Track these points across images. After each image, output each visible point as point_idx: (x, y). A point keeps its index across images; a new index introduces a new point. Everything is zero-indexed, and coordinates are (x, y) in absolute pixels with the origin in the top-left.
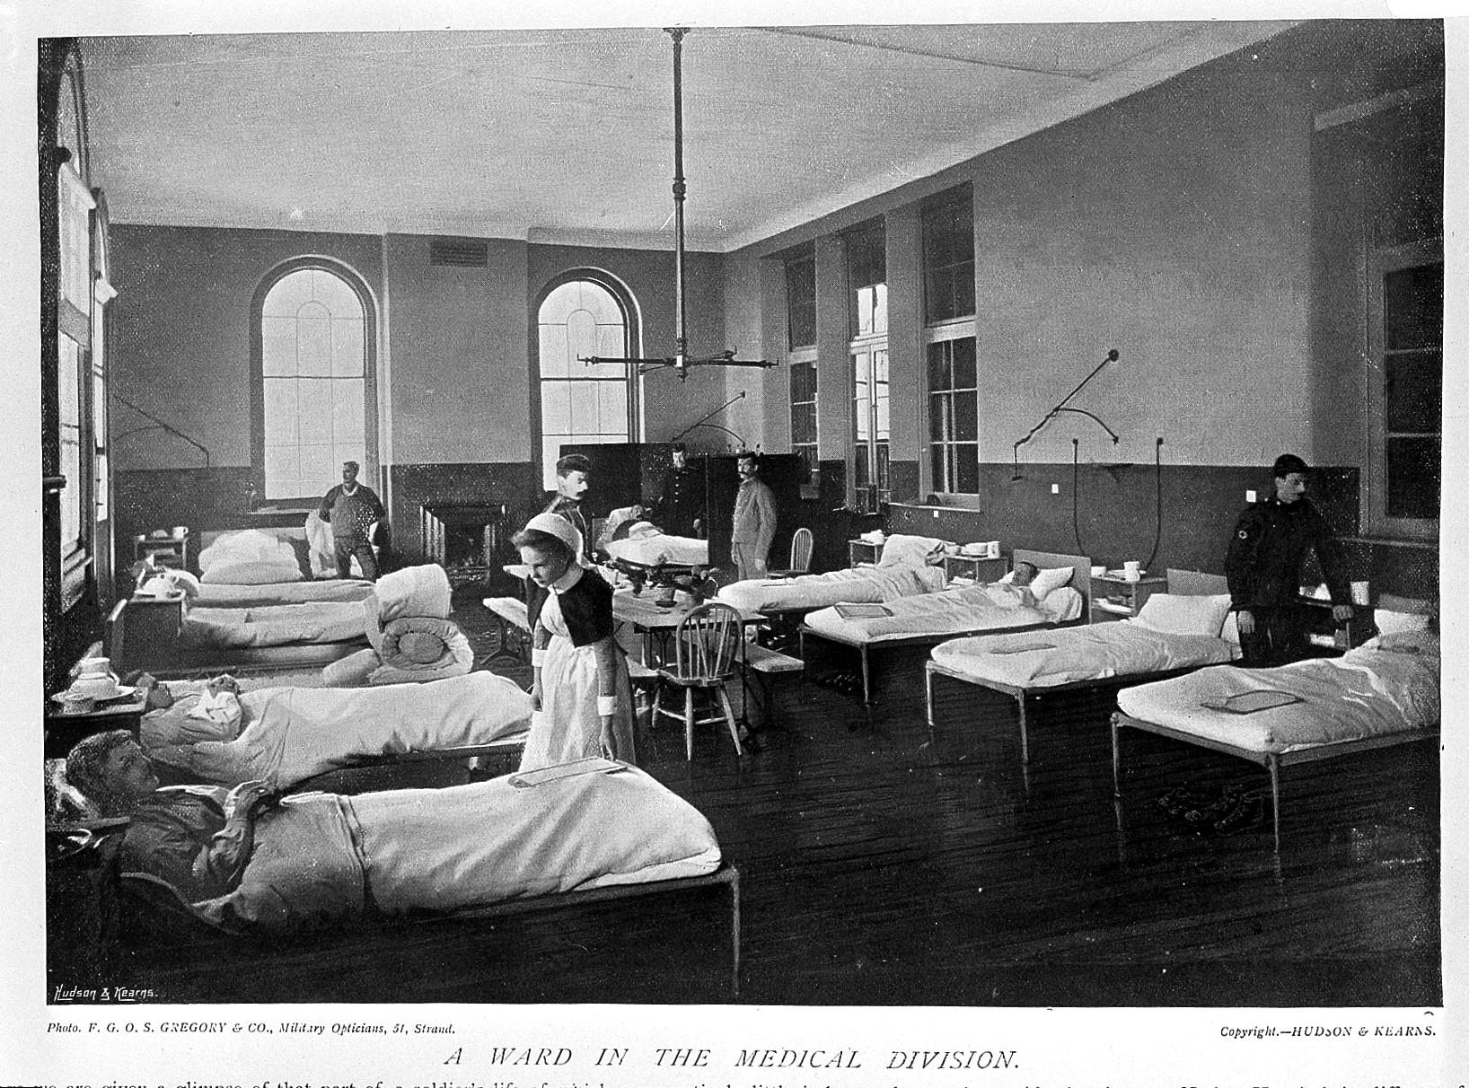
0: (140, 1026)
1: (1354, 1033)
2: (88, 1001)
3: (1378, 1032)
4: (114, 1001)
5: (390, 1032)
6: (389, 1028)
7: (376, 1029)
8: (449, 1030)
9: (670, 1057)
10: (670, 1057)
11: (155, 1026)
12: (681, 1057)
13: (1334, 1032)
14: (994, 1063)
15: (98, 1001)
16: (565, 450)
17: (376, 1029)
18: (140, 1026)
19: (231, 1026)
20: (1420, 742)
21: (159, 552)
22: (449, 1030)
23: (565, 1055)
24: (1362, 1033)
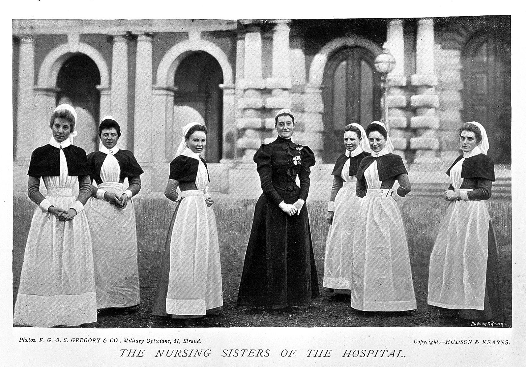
0: (62, 340)
1: (473, 342)
2: (504, 327)
3: (49, 341)
4: (491, 326)
5: (182, 343)
6: (172, 341)
7: (166, 341)
8: (199, 341)
9: (313, 353)
10: (313, 353)
11: (69, 340)
12: (319, 353)
13: (90, 340)
14: (203, 352)
15: (487, 327)
16: (264, 78)
17: (166, 341)
18: (62, 340)
19: (102, 340)
20: (496, 252)
21: (336, 44)
22: (199, 341)
23: (284, 354)
24: (105, 341)
